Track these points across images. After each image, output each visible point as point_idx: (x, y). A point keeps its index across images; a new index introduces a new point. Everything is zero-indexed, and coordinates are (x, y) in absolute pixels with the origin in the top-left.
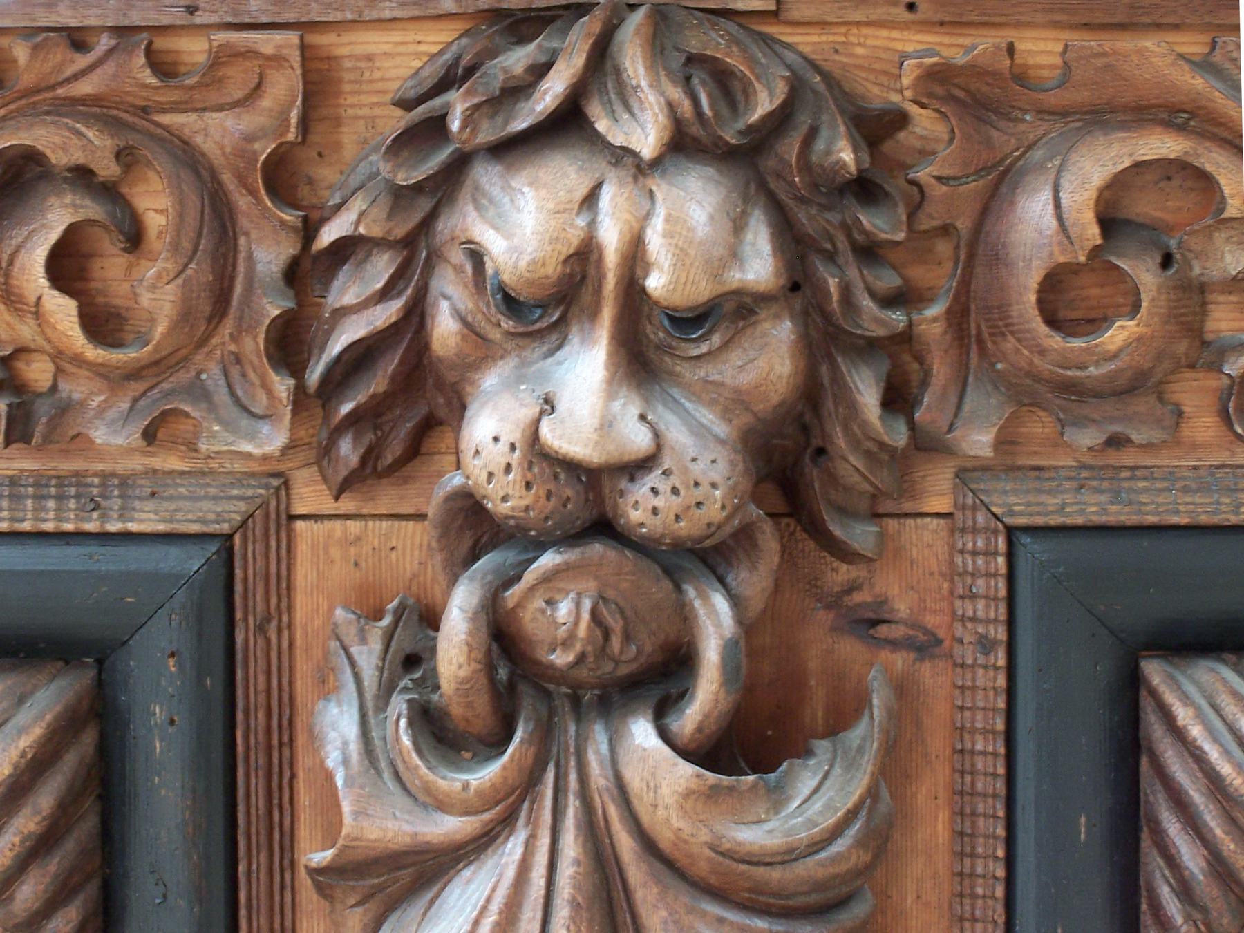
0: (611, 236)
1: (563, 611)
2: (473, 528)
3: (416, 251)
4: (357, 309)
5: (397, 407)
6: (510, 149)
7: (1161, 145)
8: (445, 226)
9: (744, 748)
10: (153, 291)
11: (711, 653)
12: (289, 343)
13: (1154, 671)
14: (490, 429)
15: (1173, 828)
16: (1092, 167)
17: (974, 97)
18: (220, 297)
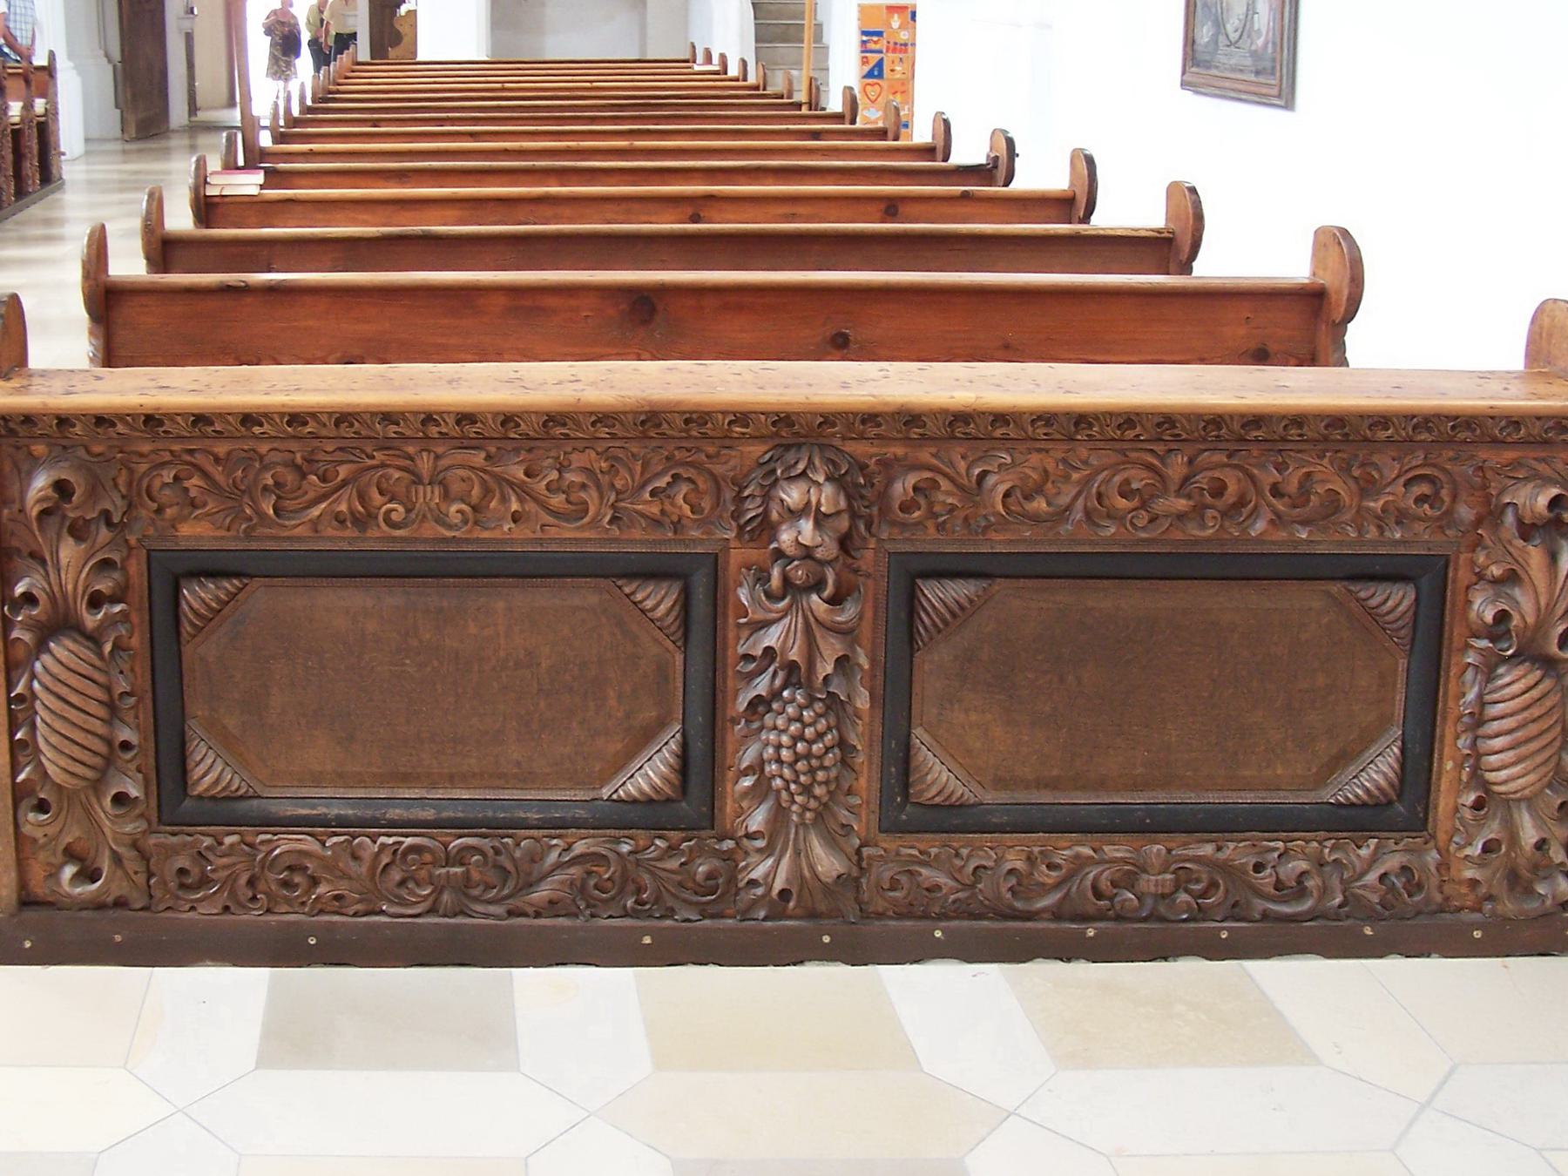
0: (814, 500)
1: (799, 574)
2: (779, 554)
3: (767, 497)
4: (752, 510)
5: (765, 529)
6: (790, 479)
7: (928, 475)
8: (773, 493)
9: (835, 601)
10: (706, 504)
11: (830, 582)
12: (736, 516)
13: (919, 582)
14: (786, 537)
15: (923, 615)
16: (912, 479)
17: (885, 464)
18: (717, 503)
